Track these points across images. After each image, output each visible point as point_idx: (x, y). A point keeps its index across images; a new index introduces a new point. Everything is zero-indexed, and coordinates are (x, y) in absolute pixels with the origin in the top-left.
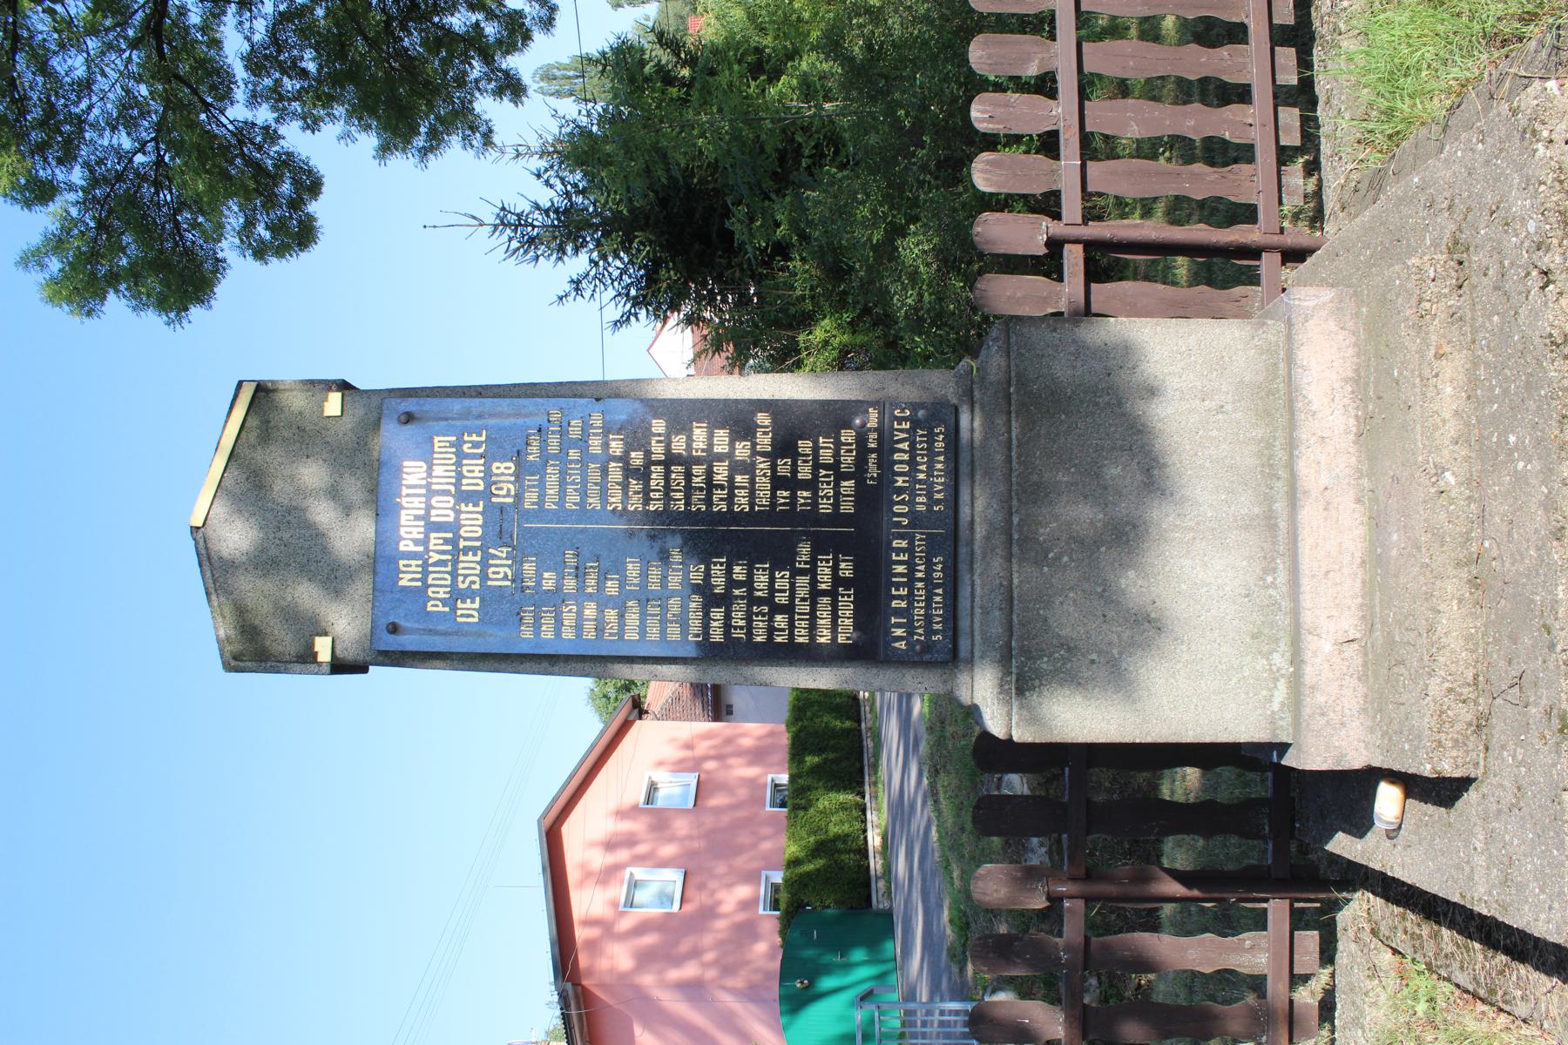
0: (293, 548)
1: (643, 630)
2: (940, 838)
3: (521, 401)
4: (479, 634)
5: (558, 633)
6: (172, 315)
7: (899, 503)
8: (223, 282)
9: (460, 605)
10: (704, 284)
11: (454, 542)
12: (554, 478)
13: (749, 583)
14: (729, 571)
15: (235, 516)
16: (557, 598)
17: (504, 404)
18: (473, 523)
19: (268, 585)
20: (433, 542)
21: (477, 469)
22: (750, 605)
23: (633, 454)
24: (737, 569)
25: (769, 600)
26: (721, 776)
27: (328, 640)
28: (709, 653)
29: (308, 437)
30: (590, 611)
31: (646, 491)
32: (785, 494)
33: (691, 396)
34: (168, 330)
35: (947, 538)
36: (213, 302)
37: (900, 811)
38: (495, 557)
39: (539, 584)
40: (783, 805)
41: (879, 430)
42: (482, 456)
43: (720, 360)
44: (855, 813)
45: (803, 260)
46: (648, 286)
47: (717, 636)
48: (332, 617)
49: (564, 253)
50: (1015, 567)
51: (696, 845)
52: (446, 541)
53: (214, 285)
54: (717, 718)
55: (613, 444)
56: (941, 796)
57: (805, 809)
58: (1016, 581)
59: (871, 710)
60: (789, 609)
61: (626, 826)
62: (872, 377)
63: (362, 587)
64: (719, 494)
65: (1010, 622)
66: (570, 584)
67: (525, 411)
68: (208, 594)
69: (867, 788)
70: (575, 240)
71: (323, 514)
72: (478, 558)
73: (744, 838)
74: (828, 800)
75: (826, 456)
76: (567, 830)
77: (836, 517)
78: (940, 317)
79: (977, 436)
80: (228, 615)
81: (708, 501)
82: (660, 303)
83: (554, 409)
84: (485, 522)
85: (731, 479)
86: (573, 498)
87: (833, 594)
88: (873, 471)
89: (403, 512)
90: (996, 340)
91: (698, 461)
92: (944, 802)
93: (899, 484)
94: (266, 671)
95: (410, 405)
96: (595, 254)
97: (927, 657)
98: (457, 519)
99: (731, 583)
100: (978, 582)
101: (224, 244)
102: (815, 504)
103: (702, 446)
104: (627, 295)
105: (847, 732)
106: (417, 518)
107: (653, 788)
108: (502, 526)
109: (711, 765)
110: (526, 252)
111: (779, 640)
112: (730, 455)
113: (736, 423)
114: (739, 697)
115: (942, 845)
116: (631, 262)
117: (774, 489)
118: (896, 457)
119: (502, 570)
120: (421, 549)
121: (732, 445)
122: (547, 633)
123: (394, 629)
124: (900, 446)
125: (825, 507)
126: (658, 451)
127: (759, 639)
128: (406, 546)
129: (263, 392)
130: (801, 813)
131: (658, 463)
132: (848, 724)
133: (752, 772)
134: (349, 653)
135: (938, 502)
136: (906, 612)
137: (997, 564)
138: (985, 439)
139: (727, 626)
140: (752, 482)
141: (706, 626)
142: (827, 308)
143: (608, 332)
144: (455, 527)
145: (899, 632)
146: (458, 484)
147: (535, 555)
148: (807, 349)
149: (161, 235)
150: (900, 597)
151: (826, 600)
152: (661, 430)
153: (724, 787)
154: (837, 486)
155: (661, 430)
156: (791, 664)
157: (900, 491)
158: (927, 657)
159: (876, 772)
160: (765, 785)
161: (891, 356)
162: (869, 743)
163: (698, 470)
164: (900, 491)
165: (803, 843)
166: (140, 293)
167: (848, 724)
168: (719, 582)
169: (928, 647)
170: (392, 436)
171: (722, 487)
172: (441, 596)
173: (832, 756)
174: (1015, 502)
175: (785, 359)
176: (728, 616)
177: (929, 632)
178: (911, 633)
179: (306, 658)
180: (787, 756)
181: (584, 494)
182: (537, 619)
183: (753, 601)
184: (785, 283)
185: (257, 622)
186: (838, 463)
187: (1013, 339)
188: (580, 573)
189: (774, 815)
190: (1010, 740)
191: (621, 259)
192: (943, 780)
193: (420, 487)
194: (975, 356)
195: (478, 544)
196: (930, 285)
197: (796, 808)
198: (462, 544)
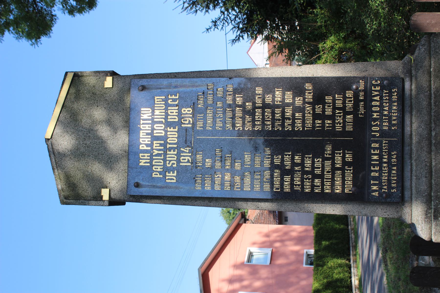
0: (91, 147)
1: (252, 187)
2: (388, 283)
3: (195, 80)
4: (176, 188)
5: (213, 187)
6: (33, 41)
7: (374, 126)
8: (55, 25)
9: (167, 174)
10: (274, 21)
11: (164, 145)
12: (210, 115)
13: (302, 164)
14: (293, 159)
15: (65, 134)
16: (212, 171)
17: (187, 81)
18: (173, 136)
19: (80, 165)
20: (155, 145)
21: (175, 111)
22: (302, 175)
23: (247, 104)
24: (297, 157)
25: (312, 172)
26: (282, 249)
27: (108, 190)
28: (279, 196)
29: (97, 97)
30: (227, 177)
31: (254, 120)
32: (319, 122)
33: (274, 76)
34: (32, 48)
35: (398, 141)
36: (51, 34)
37: (368, 269)
38: (183, 152)
39: (204, 164)
40: (311, 264)
41: (365, 91)
42: (177, 105)
43: (281, 57)
44: (346, 269)
45: (321, 8)
46: (248, 23)
47: (287, 189)
48: (109, 180)
49: (209, 8)
50: (433, 157)
51: (271, 281)
52: (161, 145)
53: (52, 27)
54: (280, 223)
55: (238, 99)
56: (389, 262)
57: (322, 266)
58: (433, 164)
59: (353, 220)
60: (321, 176)
61: (238, 272)
62: (360, 65)
63: (122, 166)
64: (288, 122)
65: (431, 183)
66: (218, 165)
67: (197, 84)
68: (53, 169)
69: (351, 257)
70: (214, 2)
71: (104, 131)
72: (176, 153)
73: (293, 279)
74: (333, 262)
75: (339, 103)
76: (212, 274)
77: (344, 133)
78: (390, 34)
79: (414, 92)
80: (62, 179)
81: (283, 125)
82: (253, 31)
83: (209, 81)
84: (179, 136)
85: (293, 115)
86: (219, 124)
87: (342, 169)
88: (362, 110)
89: (141, 131)
90: (423, 45)
91: (278, 107)
92: (390, 266)
93: (374, 117)
94: (79, 204)
95: (144, 82)
96: (223, 9)
97: (389, 200)
98: (166, 134)
99: (294, 164)
100: (414, 164)
101: (55, 8)
102: (334, 126)
103: (279, 99)
104: (238, 27)
105: (342, 230)
106: (147, 134)
107: (251, 255)
108: (187, 138)
109: (277, 245)
110: (191, 8)
111: (317, 191)
112: (293, 104)
113: (296, 88)
114: (290, 215)
115: (389, 286)
116: (240, 12)
117: (314, 120)
118: (373, 103)
119: (187, 158)
120: (149, 148)
121: (294, 98)
122: (208, 187)
123: (137, 185)
124: (375, 98)
125: (339, 128)
126: (259, 102)
127: (307, 191)
128: (143, 147)
129: (77, 77)
130: (320, 268)
131: (259, 108)
132: (342, 226)
133: (296, 248)
134: (116, 196)
135: (394, 125)
136: (378, 178)
137: (424, 155)
138: (418, 94)
139: (292, 184)
140: (304, 116)
141: (282, 184)
142: (332, 30)
143: (230, 45)
144: (165, 138)
145: (375, 188)
146: (166, 118)
147: (202, 151)
148: (323, 50)
149: (27, 5)
150: (376, 171)
151: (339, 172)
152: (260, 92)
153: (283, 255)
154: (344, 118)
155: (260, 92)
156: (322, 203)
157: (375, 120)
158: (389, 200)
159: (356, 250)
160: (303, 254)
161: (362, 55)
162: (352, 236)
163: (278, 111)
164: (375, 120)
165: (321, 282)
166: (19, 31)
167: (342, 226)
168: (288, 164)
169: (389, 195)
170: (135, 96)
171: (289, 119)
172: (159, 170)
173: (334, 241)
174: (433, 125)
175: (312, 57)
176: (292, 180)
177: (390, 188)
178: (381, 189)
179: (98, 198)
180: (314, 242)
181: (224, 123)
182: (203, 180)
183: (304, 172)
184: (312, 20)
185: (75, 182)
186: (345, 107)
187: (433, 44)
188: (222, 160)
189: (307, 269)
190: (431, 241)
191: (235, 10)
192: (389, 255)
193: (149, 120)
194: (412, 54)
195: (175, 146)
196: (384, 19)
197: (317, 266)
198: (168, 146)
